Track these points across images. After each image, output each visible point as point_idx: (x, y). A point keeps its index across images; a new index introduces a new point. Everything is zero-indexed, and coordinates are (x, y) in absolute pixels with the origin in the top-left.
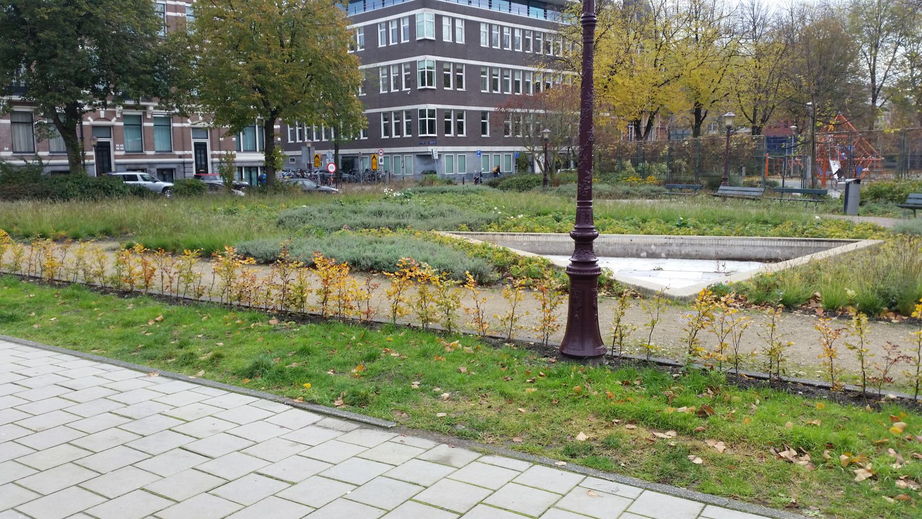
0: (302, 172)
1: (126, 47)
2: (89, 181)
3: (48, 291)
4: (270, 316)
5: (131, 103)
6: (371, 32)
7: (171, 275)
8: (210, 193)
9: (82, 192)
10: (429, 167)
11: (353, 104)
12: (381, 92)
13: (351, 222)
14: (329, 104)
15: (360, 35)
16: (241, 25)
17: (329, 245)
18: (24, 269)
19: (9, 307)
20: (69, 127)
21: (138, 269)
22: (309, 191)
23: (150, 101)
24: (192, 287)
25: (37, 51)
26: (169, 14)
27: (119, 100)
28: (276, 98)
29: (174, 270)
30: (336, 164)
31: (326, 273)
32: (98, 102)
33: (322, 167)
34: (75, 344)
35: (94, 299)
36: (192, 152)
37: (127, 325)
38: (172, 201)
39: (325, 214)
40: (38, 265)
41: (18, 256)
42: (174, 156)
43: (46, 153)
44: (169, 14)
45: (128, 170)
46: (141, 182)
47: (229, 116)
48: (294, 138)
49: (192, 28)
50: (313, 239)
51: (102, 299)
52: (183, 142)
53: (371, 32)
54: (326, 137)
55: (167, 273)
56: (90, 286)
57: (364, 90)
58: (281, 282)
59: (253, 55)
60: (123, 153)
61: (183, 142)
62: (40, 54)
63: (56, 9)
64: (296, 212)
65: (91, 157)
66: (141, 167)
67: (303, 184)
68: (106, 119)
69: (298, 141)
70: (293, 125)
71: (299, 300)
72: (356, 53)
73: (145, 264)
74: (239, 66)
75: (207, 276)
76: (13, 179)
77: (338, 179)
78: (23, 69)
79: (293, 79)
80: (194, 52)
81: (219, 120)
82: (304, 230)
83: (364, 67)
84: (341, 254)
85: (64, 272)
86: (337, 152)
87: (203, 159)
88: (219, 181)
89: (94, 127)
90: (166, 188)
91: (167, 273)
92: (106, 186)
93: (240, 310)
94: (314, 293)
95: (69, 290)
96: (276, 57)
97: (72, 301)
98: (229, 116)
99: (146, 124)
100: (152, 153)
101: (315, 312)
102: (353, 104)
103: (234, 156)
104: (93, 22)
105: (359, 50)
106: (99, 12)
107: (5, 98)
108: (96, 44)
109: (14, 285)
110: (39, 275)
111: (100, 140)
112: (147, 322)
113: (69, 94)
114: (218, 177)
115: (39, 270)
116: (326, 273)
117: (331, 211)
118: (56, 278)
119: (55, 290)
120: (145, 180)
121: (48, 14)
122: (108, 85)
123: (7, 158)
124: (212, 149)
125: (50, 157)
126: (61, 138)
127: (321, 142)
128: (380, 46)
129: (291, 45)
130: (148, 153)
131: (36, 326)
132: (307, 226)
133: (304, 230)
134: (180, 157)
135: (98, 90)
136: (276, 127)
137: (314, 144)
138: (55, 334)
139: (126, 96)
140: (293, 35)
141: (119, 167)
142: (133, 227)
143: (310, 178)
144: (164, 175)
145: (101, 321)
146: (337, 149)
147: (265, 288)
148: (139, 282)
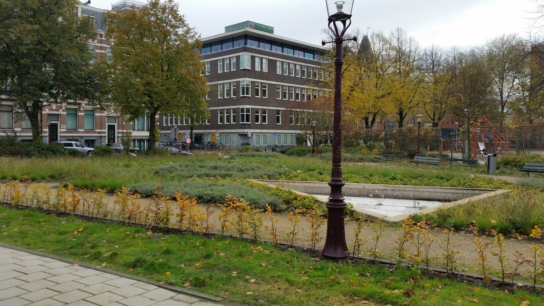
2: (44, 146)
3: (14, 212)
4: (148, 230)
5: (72, 101)
6: (214, 65)
7: (89, 203)
8: (115, 154)
9: (39, 152)
10: (246, 141)
11: (202, 104)
12: (219, 98)
13: (198, 173)
14: (188, 104)
15: (208, 66)
16: (139, 59)
17: (185, 186)
20: (34, 115)
21: (70, 200)
22: (174, 154)
23: (82, 100)
24: (101, 211)
27: (64, 99)
29: (91, 201)
30: (191, 138)
31: (182, 204)
34: (28, 245)
35: (42, 217)
36: (106, 130)
37: (61, 233)
39: (184, 168)
40: (9, 196)
42: (96, 132)
43: (19, 129)
45: (68, 140)
46: (75, 147)
48: (167, 123)
49: (110, 60)
50: (175, 183)
51: (47, 218)
52: (101, 125)
53: (214, 65)
54: (186, 123)
55: (87, 202)
56: (40, 209)
60: (65, 130)
61: (101, 125)
62: (20, 72)
63: (31, 47)
64: (166, 167)
65: (46, 132)
66: (75, 138)
68: (56, 110)
69: (169, 125)
71: (165, 220)
72: (205, 76)
73: (74, 197)
74: (137, 82)
75: (111, 204)
77: (192, 147)
78: (9, 80)
79: (168, 89)
80: (110, 73)
81: (123, 112)
83: (210, 84)
85: (24, 200)
88: (121, 147)
89: (49, 115)
90: (89, 151)
91: (87, 202)
92: (54, 149)
93: (129, 226)
94: (175, 215)
95: (27, 212)
96: (158, 77)
97: (29, 218)
98: (129, 110)
99: (79, 114)
100: (83, 130)
102: (202, 104)
104: (52, 54)
105: (207, 74)
106: (56, 49)
108: (53, 67)
110: (9, 202)
112: (73, 232)
113: (35, 95)
114: (121, 145)
115: (10, 199)
117: (187, 166)
118: (20, 204)
119: (19, 212)
120: (77, 146)
121: (26, 49)
122: (59, 90)
124: (118, 129)
126: (29, 121)
128: (219, 72)
129: (168, 71)
130: (80, 130)
131: (5, 234)
132: (172, 175)
133: (171, 177)
134: (99, 133)
135: (52, 93)
137: (178, 127)
138: (16, 238)
139: (69, 97)
140: (169, 65)
141: (62, 138)
142: (68, 174)
144: (89, 144)
145: (45, 231)
147: (145, 212)
148: (70, 207)
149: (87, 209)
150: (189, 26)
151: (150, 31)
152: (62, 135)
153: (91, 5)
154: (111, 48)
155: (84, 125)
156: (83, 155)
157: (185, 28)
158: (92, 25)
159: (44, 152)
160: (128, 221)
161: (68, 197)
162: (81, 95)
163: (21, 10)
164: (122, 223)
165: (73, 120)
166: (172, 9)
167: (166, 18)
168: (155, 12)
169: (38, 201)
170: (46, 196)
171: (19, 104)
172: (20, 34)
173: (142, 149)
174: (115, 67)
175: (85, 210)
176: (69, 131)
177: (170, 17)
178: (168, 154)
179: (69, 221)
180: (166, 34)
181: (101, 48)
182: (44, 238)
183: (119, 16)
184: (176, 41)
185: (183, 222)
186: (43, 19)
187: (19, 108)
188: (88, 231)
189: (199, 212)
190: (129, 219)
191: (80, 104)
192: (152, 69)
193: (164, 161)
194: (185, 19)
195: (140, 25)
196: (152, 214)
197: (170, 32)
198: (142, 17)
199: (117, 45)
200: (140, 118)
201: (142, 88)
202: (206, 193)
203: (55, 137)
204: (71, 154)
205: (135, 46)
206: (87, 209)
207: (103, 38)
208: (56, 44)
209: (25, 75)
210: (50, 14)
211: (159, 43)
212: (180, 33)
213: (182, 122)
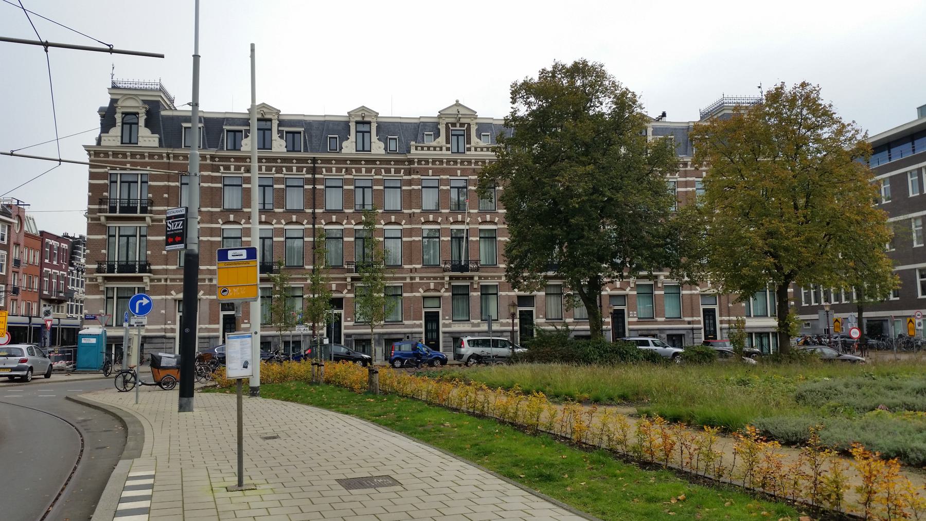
0: (819, 337)
1: (642, 224)
2: (606, 346)
3: (578, 454)
4: (800, 510)
5: (645, 273)
6: (899, 183)
7: (691, 451)
8: (720, 360)
9: (601, 356)
11: (880, 262)
12: (915, 245)
13: (889, 401)
14: (851, 264)
15: (885, 189)
16: (752, 193)
17: (863, 428)
18: (557, 429)
19: (547, 465)
20: (591, 298)
21: (659, 441)
22: (830, 360)
23: (660, 270)
24: (712, 467)
25: (568, 234)
26: (680, 189)
27: (633, 272)
28: (790, 262)
29: (694, 446)
30: (860, 328)
31: (867, 468)
32: (616, 274)
33: (844, 332)
34: (603, 513)
35: (618, 468)
36: (701, 319)
37: (651, 500)
38: (683, 368)
39: (853, 389)
40: (568, 427)
41: (553, 416)
42: (683, 322)
43: (571, 320)
44: (680, 189)
45: (640, 336)
46: (652, 347)
47: (739, 282)
48: (808, 300)
49: (702, 201)
50: (841, 419)
51: (625, 469)
52: (692, 309)
53: (899, 183)
54: (847, 299)
55: (687, 447)
56: (613, 452)
57: (893, 245)
58: (812, 473)
59: (765, 220)
60: (635, 320)
61: (692, 309)
62: (570, 236)
63: (585, 198)
64: (817, 386)
65: (608, 324)
66: (653, 332)
67: (822, 353)
68: (621, 289)
69: (813, 304)
70: (806, 287)
71: (834, 497)
72: (881, 206)
73: (665, 437)
74: (750, 232)
75: (727, 453)
76: (547, 343)
77: (863, 346)
78: (557, 249)
79: (808, 240)
80: (703, 223)
81: (728, 286)
82: (829, 407)
83: (892, 220)
84: (880, 441)
85: (590, 436)
86: (860, 314)
87: (712, 325)
88: (729, 347)
89: (611, 296)
90: (676, 354)
91: (687, 447)
92: (621, 351)
93: (764, 498)
94: (852, 490)
95: (595, 455)
96: (789, 220)
97: (599, 467)
98: (739, 282)
99: (657, 292)
100: (663, 319)
101: (854, 513)
102: (880, 262)
103: (743, 322)
104: (614, 205)
105: (884, 202)
106: (619, 197)
107: (543, 274)
108: (615, 223)
109: (550, 444)
110: (569, 436)
111: (616, 308)
112: (670, 499)
113: (592, 268)
114: (728, 344)
115: (569, 431)
116: (867, 468)
117: (859, 386)
118: (584, 440)
119: (583, 454)
120: (656, 345)
121: (578, 203)
122: (625, 259)
123: (541, 324)
124: (721, 315)
125: (577, 323)
126: (584, 307)
127: (840, 304)
128: (911, 195)
129: (806, 207)
130: (659, 319)
131: (569, 489)
132: (832, 403)
133: (829, 407)
134: (689, 323)
135: (616, 264)
136: (790, 290)
137: (833, 307)
138: (586, 500)
139: (640, 268)
140: (808, 197)
141: (633, 333)
142: (648, 393)
143: (829, 345)
144: (674, 341)
145: (625, 492)
146: (860, 310)
147: (792, 477)
148: (660, 454)
149: (689, 460)
150: (843, 121)
151: (769, 142)
152: (631, 327)
153: (667, 119)
154: (703, 182)
155: (664, 311)
156: (669, 360)
157: (835, 126)
158: (670, 152)
159: (608, 355)
160: (761, 489)
161: (657, 435)
162: (659, 263)
163: (570, 148)
164: (750, 493)
165: (650, 305)
166: (807, 97)
167: (797, 115)
168: (776, 109)
169: (610, 440)
170: (621, 432)
171: (571, 283)
172: (570, 182)
173: (765, 351)
174: (711, 214)
175: (685, 461)
176: (641, 321)
177: (805, 112)
178: (818, 360)
179: (661, 480)
180: (799, 143)
181: (686, 184)
182: (626, 504)
183: (714, 127)
184: (818, 151)
185: (873, 504)
186: (598, 155)
187: (571, 289)
188: (694, 500)
189: (907, 489)
190: (763, 486)
191: (472, 278)
192: (777, 208)
193: (811, 374)
194: (833, 110)
195: (752, 136)
196: (807, 483)
197: (808, 138)
198: (755, 122)
199: (712, 176)
200: (759, 296)
201: (761, 243)
202: (913, 445)
203: (621, 330)
204: (648, 360)
205: (743, 172)
206: (689, 460)
207: (689, 168)
208: (617, 189)
209: (577, 240)
210: (609, 145)
211: (788, 161)
212: (826, 136)
213: (838, 298)
